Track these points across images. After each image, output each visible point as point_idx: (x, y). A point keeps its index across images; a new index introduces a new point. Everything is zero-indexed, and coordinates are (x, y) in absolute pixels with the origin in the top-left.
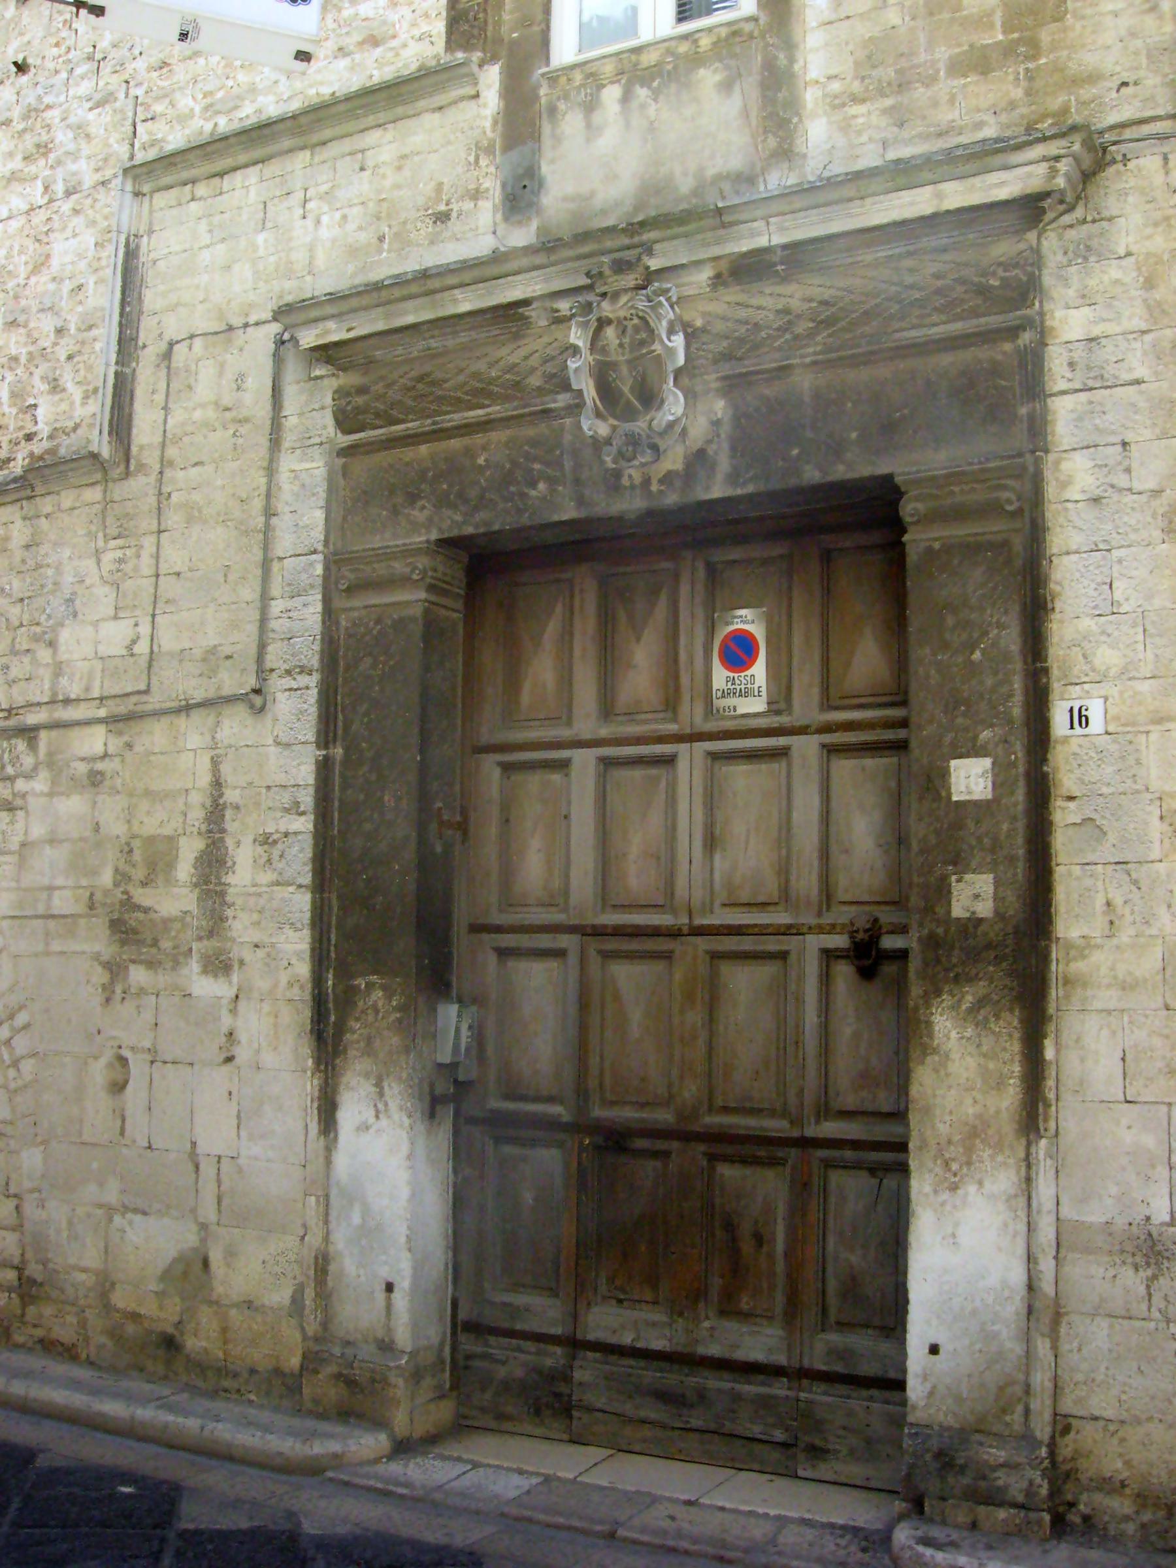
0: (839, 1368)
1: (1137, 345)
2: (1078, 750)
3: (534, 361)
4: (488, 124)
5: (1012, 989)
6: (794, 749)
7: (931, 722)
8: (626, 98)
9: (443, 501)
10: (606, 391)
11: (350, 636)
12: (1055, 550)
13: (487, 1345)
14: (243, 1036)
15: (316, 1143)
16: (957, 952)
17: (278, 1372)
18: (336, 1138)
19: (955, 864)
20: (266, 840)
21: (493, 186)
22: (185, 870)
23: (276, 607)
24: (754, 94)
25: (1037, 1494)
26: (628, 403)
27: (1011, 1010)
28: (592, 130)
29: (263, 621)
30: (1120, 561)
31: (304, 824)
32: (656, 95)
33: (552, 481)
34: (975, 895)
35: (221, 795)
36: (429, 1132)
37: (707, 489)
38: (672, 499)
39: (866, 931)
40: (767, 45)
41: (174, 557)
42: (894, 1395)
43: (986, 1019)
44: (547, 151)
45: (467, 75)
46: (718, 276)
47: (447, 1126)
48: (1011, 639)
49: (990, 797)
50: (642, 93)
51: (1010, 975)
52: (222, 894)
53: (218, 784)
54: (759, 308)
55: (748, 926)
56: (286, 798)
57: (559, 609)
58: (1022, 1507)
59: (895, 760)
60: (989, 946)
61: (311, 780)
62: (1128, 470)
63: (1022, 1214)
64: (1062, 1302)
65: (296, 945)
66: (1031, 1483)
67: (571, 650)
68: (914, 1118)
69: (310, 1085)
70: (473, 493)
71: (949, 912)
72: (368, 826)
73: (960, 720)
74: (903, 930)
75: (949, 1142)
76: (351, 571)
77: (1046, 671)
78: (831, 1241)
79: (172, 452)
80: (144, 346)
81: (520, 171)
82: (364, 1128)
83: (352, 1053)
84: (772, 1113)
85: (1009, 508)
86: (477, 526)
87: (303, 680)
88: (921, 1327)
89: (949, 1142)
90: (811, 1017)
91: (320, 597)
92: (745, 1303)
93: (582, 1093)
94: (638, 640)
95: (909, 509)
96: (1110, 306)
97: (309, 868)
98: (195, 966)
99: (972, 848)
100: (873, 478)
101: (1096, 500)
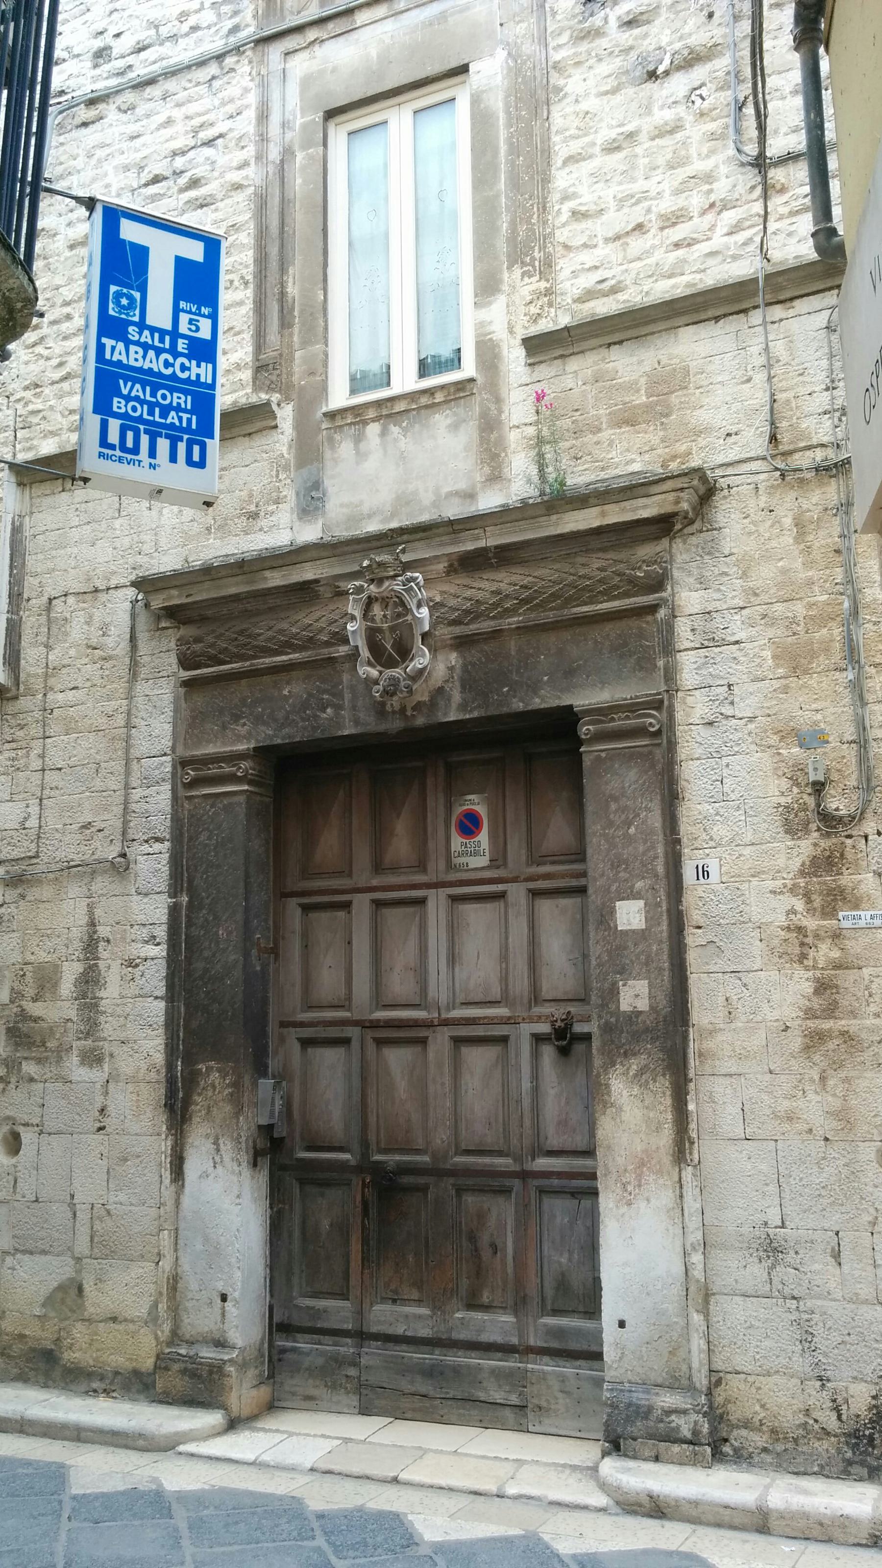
0: (555, 1344)
1: (736, 617)
2: (703, 895)
3: (322, 624)
4: (284, 450)
5: (663, 1060)
6: (509, 893)
7: (603, 875)
8: (384, 433)
9: (258, 720)
10: (375, 647)
11: (193, 816)
12: (683, 757)
13: (295, 1341)
14: (111, 1109)
15: (168, 1192)
16: (625, 1034)
17: (136, 1373)
18: (183, 1186)
19: (621, 974)
20: (131, 964)
21: (289, 493)
22: (67, 986)
23: (136, 794)
24: (475, 436)
25: (701, 1432)
26: (390, 654)
27: (664, 1075)
28: (361, 456)
29: (126, 803)
30: (727, 766)
31: (160, 951)
32: (405, 431)
33: (338, 707)
34: (636, 995)
35: (95, 932)
36: (253, 1177)
37: (445, 714)
38: (420, 721)
39: (562, 1020)
40: (483, 399)
41: (56, 758)
42: (596, 1364)
43: (647, 1082)
44: (329, 472)
45: (268, 412)
46: (451, 565)
47: (266, 1172)
48: (655, 820)
49: (644, 927)
50: (395, 430)
51: (661, 1050)
52: (96, 1005)
53: (92, 924)
54: (479, 589)
55: (479, 1018)
56: (145, 933)
57: (341, 793)
58: (691, 1443)
59: (579, 900)
60: (647, 1030)
61: (164, 919)
62: (732, 703)
63: (678, 1221)
64: (711, 1286)
65: (152, 1045)
66: (696, 1423)
67: (351, 824)
68: (599, 1153)
69: (165, 1145)
70: (280, 715)
71: (618, 1007)
72: (206, 954)
73: (622, 874)
74: (588, 1019)
75: (625, 1170)
76: (192, 770)
77: (679, 841)
78: (545, 1248)
79: (52, 682)
80: (29, 600)
81: (309, 484)
82: (205, 1175)
83: (196, 1120)
84: (500, 1153)
85: (652, 729)
86: (283, 738)
87: (157, 847)
88: (611, 1306)
89: (625, 1170)
90: (526, 1085)
91: (170, 787)
92: (485, 1298)
93: (365, 1144)
94: (398, 816)
95: (585, 729)
96: (719, 590)
97: (164, 983)
98: (75, 1060)
99: (632, 962)
100: (559, 708)
101: (710, 724)
